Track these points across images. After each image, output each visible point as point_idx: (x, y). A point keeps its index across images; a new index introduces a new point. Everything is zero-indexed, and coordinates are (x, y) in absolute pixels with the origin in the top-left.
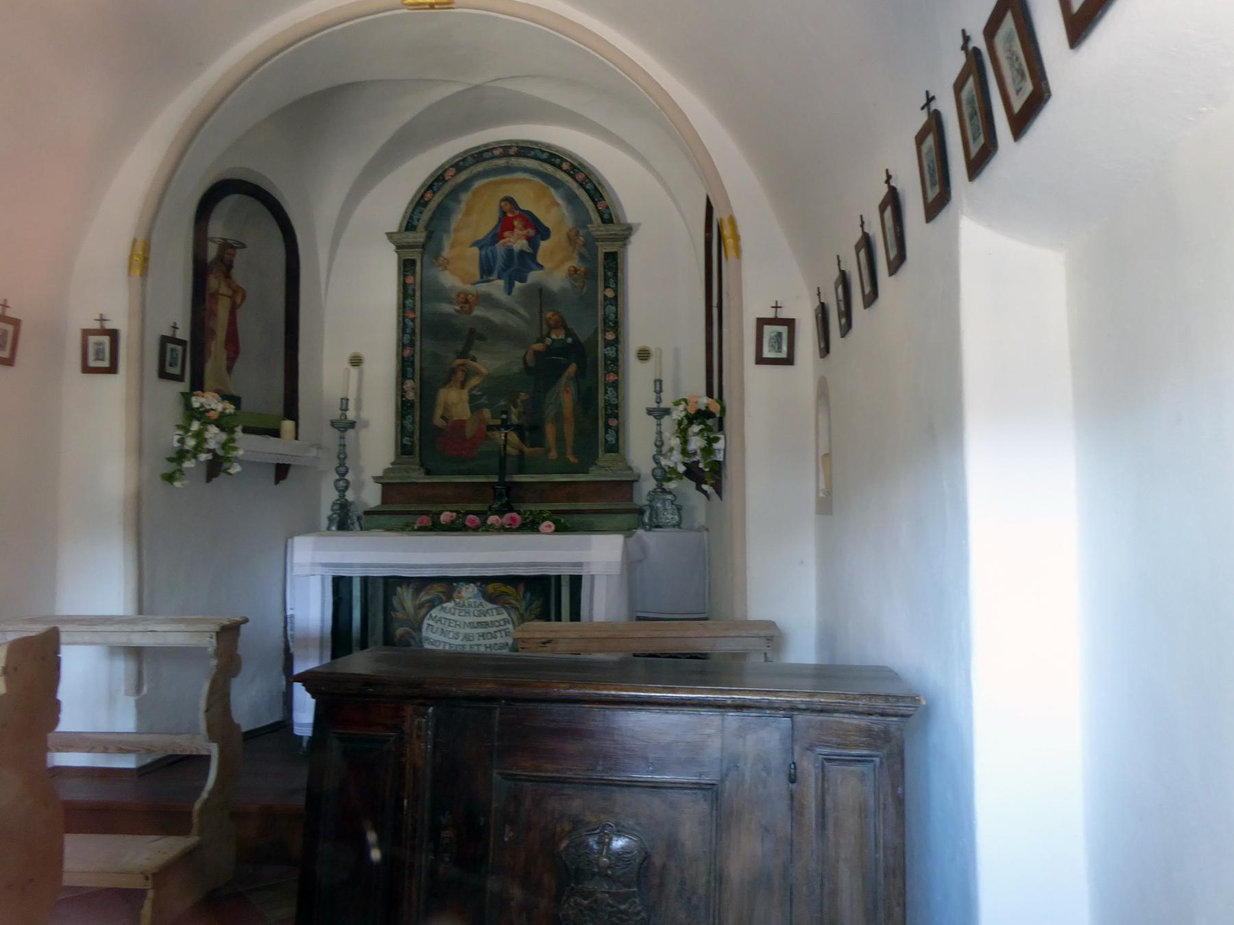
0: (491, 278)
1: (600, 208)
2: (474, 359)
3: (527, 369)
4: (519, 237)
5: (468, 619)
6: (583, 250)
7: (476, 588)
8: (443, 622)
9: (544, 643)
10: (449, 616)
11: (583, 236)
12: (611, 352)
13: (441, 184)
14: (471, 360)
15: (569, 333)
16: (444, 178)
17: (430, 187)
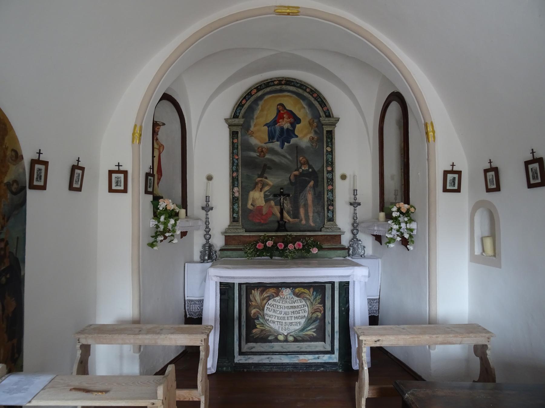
0: (274, 141)
1: (324, 110)
2: (266, 178)
3: (291, 182)
4: (287, 122)
5: (286, 305)
6: (316, 129)
7: (290, 290)
8: (274, 306)
9: (375, 341)
10: (278, 304)
11: (316, 122)
12: (330, 176)
13: (250, 96)
14: (265, 178)
15: (310, 167)
16: (251, 94)
17: (245, 98)
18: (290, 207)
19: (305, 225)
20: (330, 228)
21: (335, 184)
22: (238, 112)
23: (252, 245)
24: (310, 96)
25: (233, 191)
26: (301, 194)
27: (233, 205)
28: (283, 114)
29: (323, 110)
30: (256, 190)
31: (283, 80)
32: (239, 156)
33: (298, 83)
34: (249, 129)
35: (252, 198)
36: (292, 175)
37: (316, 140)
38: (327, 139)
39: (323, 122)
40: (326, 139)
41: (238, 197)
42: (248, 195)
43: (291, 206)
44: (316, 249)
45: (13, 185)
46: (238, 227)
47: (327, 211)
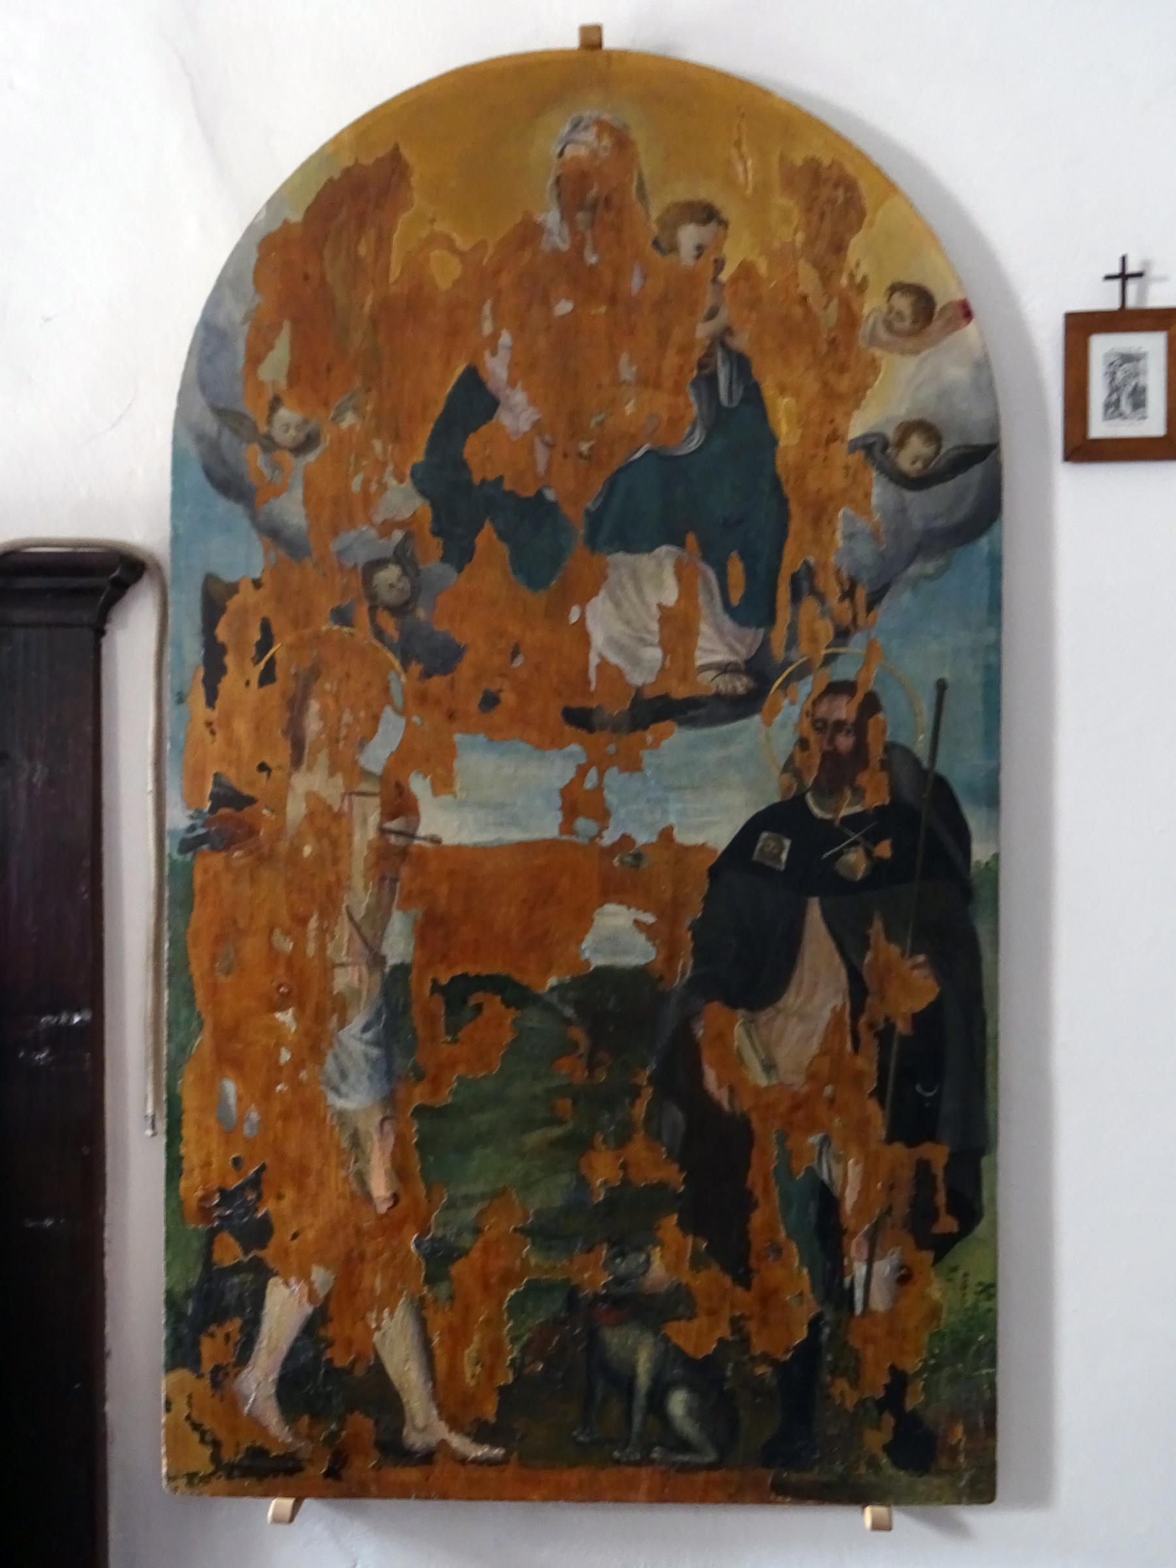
45: (901, 443)
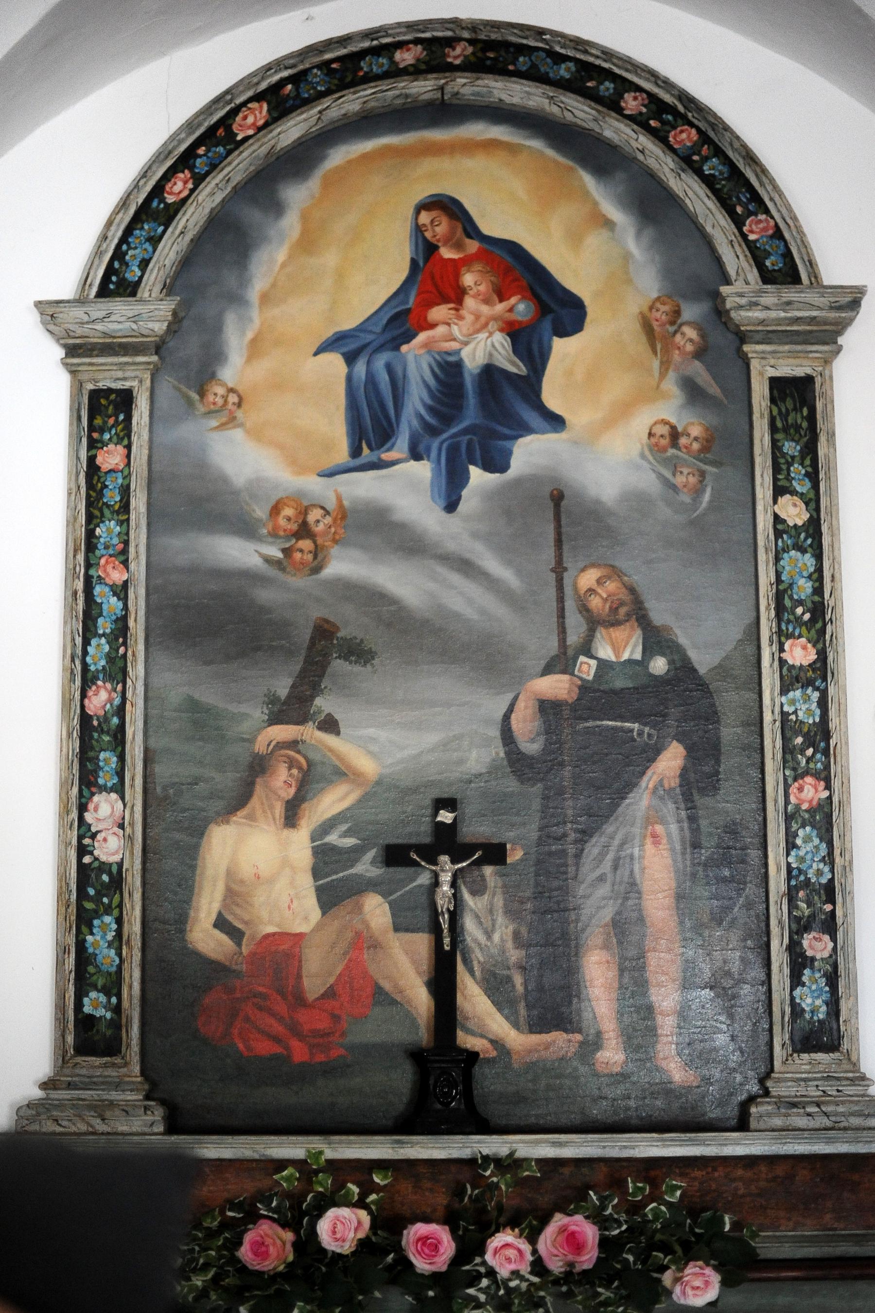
0: (386, 456)
1: (752, 237)
2: (330, 725)
6: (698, 370)
13: (220, 149)
14: (320, 728)
17: (186, 160)
18: (510, 944)
19: (623, 1077)
20: (818, 1105)
21: (846, 768)
22: (134, 255)
23: (211, 1234)
24: (644, 141)
25: (81, 818)
26: (593, 848)
27: (84, 929)
28: (456, 267)
29: (744, 236)
30: (251, 817)
31: (460, 39)
32: (132, 566)
33: (565, 58)
34: (213, 376)
35: (222, 870)
36: (521, 704)
37: (696, 446)
38: (779, 436)
39: (746, 317)
40: (774, 443)
41: (120, 865)
42: (196, 847)
43: (516, 935)
44: (708, 1271)
46: (114, 1095)
47: (787, 971)
